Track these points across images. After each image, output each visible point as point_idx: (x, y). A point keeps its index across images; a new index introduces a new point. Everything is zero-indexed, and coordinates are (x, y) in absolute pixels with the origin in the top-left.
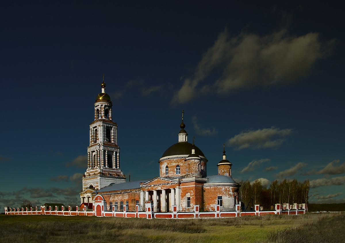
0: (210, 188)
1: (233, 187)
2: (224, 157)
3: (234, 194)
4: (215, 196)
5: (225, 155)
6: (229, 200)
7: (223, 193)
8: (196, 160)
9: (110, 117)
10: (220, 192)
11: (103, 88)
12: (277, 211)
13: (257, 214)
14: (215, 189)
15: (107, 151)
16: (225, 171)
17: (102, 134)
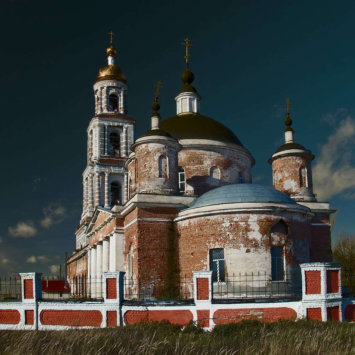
1: (263, 216)
2: (288, 137)
3: (271, 240)
4: (203, 249)
5: (291, 130)
7: (226, 239)
8: (151, 145)
9: (120, 108)
10: (217, 236)
11: (110, 56)
12: (307, 301)
13: (203, 315)
14: (201, 226)
15: (107, 175)
16: (286, 176)
17: (98, 142)
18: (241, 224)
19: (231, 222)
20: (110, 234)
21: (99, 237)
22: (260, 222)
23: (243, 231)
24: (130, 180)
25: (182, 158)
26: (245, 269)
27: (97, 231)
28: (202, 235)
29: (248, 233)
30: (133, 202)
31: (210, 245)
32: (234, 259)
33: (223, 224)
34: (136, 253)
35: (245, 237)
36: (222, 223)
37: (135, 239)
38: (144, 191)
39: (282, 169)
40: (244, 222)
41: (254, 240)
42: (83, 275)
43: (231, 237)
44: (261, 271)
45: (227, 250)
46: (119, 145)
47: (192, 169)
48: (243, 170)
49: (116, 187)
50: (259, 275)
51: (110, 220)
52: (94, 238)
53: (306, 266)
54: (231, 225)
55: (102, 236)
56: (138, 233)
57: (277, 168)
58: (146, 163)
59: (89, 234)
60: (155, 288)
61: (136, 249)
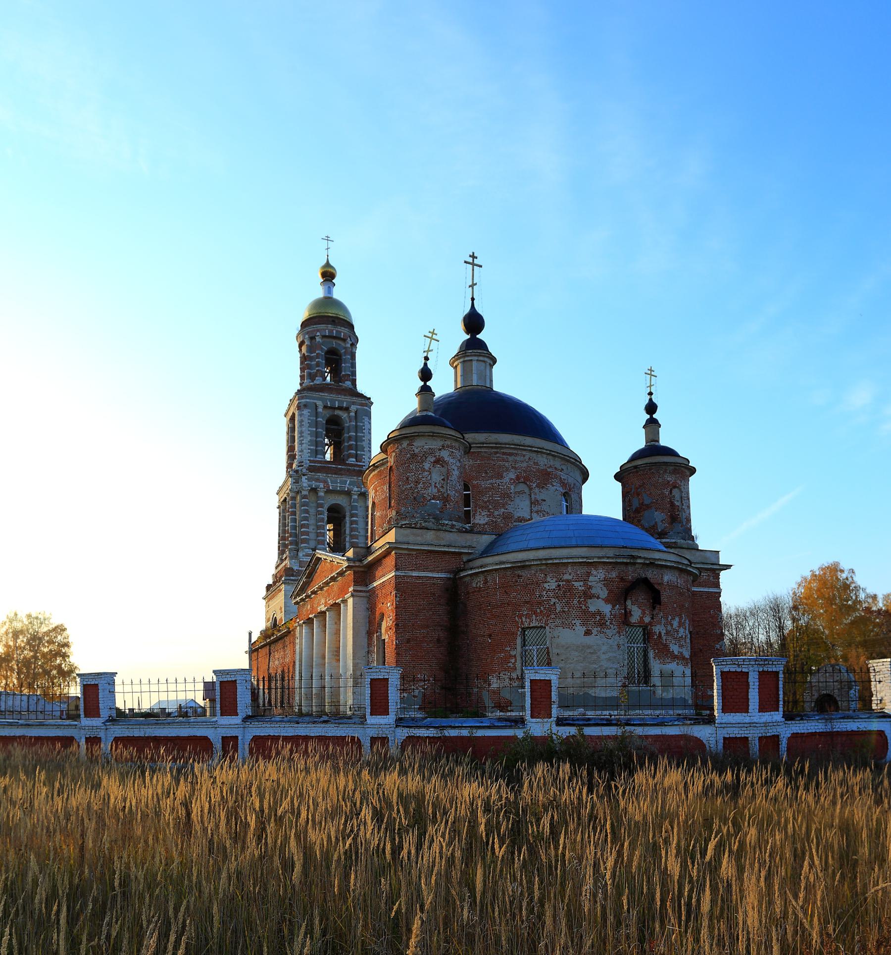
0: (486, 582)
6: (589, 647)
7: (551, 610)
18: (576, 584)
19: (559, 581)
20: (341, 599)
21: (318, 603)
22: (607, 582)
23: (580, 597)
24: (374, 503)
25: (467, 467)
26: (582, 665)
27: (314, 592)
28: (508, 603)
29: (589, 601)
30: (388, 543)
31: (522, 621)
32: (563, 646)
33: (546, 585)
34: (392, 633)
35: (583, 607)
36: (543, 582)
37: (390, 608)
38: (405, 524)
39: (639, 490)
40: (582, 581)
41: (599, 613)
42: (283, 671)
43: (558, 609)
44: (610, 668)
45: (551, 630)
46: (341, 441)
47: (483, 486)
48: (570, 490)
49: (336, 515)
50: (661, 677)
51: (341, 574)
52: (309, 606)
53: (722, 663)
54: (559, 586)
55: (326, 603)
56: (396, 597)
57: (631, 489)
58: (408, 474)
59: (298, 599)
60: (424, 695)
61: (391, 625)
